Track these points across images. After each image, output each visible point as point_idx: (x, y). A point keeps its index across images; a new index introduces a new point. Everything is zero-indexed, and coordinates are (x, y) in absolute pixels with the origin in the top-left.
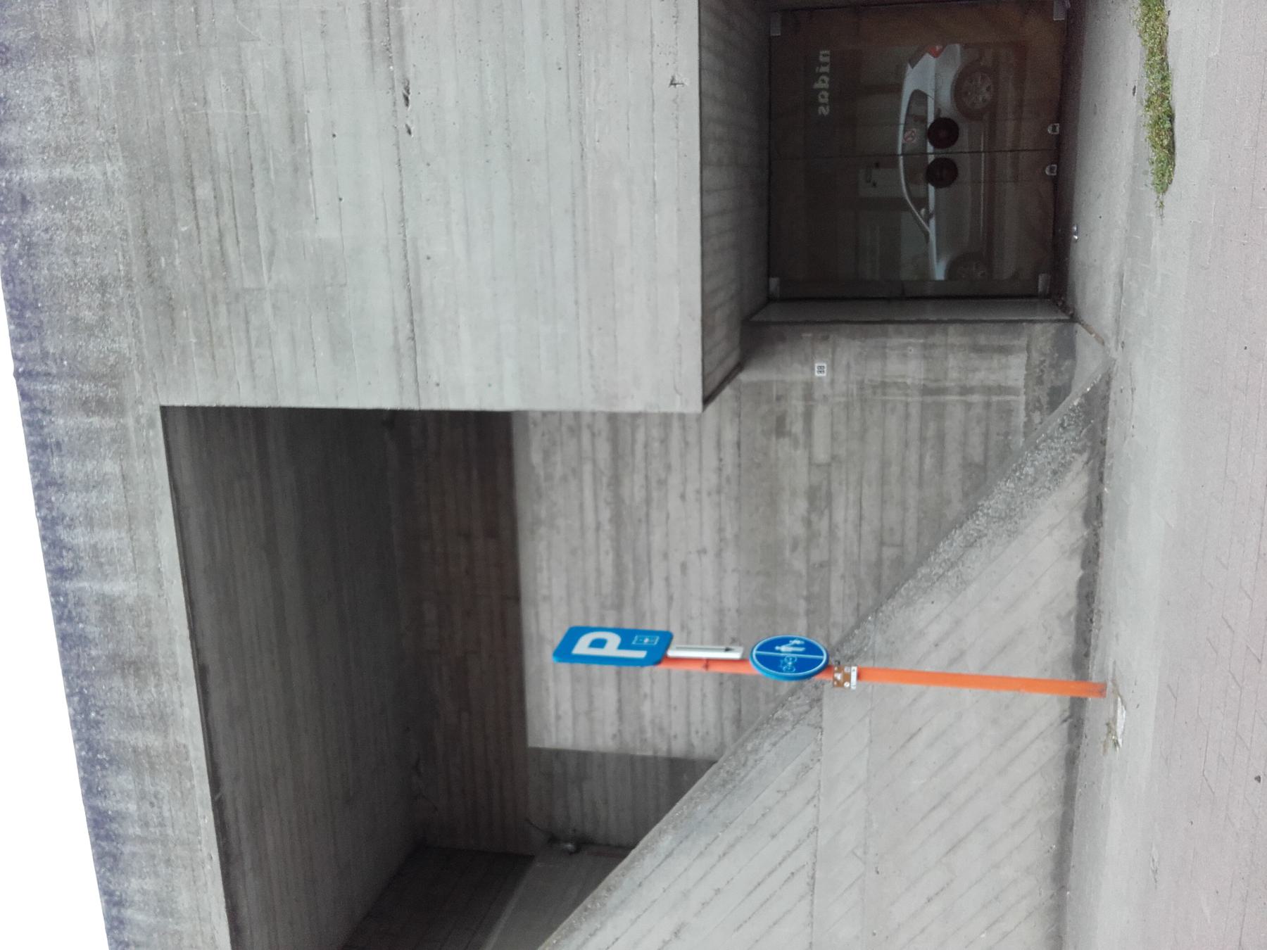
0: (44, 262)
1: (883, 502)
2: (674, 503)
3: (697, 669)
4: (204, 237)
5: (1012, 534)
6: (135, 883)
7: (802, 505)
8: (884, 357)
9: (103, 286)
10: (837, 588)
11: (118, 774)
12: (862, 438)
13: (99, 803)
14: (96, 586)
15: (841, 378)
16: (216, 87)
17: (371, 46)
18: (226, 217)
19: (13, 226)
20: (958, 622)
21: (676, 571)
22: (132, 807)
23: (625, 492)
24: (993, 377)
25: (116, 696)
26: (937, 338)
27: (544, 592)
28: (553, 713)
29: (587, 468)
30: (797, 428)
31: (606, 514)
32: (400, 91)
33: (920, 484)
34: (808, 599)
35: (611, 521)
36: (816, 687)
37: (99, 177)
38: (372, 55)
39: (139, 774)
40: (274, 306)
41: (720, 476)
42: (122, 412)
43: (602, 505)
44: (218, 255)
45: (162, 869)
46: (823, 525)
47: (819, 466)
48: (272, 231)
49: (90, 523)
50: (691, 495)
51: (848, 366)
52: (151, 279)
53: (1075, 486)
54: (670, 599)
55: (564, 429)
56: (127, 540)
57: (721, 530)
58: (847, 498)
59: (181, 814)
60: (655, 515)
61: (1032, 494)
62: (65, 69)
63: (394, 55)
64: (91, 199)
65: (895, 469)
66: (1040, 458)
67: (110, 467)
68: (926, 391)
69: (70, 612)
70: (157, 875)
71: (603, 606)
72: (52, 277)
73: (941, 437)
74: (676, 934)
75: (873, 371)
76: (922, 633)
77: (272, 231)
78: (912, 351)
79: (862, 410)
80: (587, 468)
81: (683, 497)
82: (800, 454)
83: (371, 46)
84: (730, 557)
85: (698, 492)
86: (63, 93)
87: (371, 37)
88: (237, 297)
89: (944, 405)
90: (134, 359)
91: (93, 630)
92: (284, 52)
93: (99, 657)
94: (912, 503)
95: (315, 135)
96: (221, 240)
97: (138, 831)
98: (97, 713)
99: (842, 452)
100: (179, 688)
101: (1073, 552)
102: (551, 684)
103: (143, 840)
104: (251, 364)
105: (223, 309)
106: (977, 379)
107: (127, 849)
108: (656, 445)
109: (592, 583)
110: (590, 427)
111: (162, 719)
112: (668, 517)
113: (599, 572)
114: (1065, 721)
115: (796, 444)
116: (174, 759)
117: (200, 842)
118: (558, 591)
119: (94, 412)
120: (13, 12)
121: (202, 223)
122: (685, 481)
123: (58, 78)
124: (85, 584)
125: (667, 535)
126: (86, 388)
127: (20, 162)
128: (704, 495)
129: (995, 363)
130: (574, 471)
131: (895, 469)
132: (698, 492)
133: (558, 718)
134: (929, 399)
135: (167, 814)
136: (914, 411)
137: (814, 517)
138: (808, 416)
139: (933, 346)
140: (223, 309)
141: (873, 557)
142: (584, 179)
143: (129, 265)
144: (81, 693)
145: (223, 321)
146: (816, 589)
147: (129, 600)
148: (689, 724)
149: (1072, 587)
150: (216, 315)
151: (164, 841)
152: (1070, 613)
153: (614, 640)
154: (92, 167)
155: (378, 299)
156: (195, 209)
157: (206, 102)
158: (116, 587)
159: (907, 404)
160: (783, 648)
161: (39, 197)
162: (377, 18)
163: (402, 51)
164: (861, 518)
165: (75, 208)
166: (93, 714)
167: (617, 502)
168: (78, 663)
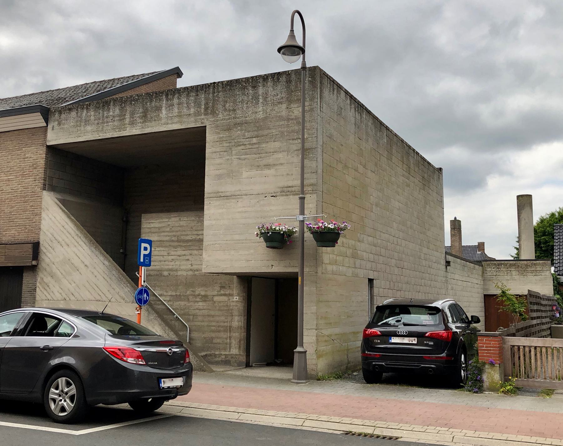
0: (240, 93)
4: (244, 140)
6: (92, 113)
7: (203, 293)
9: (234, 110)
10: (182, 303)
12: (219, 310)
14: (164, 105)
15: (234, 304)
16: (277, 144)
18: (248, 146)
21: (187, 258)
22: (111, 113)
26: (243, 330)
32: (274, 195)
33: (208, 326)
34: (180, 295)
39: (119, 116)
42: (205, 115)
45: (96, 122)
46: (198, 300)
48: (245, 159)
49: (179, 104)
52: (236, 124)
54: (180, 256)
56: (175, 115)
65: (211, 319)
67: (192, 110)
68: (230, 327)
70: (95, 120)
73: (219, 331)
74: (86, 265)
75: (236, 313)
76: (154, 328)
77: (245, 159)
84: (190, 273)
89: (227, 332)
91: (153, 104)
94: (203, 324)
95: (267, 172)
97: (105, 115)
99: (216, 304)
103: (103, 117)
104: (215, 152)
105: (228, 145)
106: (233, 341)
107: (101, 111)
109: (184, 233)
111: (132, 123)
118: (182, 223)
123: (282, 98)
124: (164, 102)
127: (264, 86)
129: (236, 346)
131: (211, 319)
133: (149, 223)
134: (228, 328)
135: (110, 124)
136: (226, 324)
138: (225, 295)
140: (228, 145)
141: (190, 313)
145: (225, 145)
146: (182, 297)
151: (103, 123)
153: (147, 252)
155: (229, 188)
158: (164, 111)
160: (145, 295)
163: (282, 195)
165: (252, 102)
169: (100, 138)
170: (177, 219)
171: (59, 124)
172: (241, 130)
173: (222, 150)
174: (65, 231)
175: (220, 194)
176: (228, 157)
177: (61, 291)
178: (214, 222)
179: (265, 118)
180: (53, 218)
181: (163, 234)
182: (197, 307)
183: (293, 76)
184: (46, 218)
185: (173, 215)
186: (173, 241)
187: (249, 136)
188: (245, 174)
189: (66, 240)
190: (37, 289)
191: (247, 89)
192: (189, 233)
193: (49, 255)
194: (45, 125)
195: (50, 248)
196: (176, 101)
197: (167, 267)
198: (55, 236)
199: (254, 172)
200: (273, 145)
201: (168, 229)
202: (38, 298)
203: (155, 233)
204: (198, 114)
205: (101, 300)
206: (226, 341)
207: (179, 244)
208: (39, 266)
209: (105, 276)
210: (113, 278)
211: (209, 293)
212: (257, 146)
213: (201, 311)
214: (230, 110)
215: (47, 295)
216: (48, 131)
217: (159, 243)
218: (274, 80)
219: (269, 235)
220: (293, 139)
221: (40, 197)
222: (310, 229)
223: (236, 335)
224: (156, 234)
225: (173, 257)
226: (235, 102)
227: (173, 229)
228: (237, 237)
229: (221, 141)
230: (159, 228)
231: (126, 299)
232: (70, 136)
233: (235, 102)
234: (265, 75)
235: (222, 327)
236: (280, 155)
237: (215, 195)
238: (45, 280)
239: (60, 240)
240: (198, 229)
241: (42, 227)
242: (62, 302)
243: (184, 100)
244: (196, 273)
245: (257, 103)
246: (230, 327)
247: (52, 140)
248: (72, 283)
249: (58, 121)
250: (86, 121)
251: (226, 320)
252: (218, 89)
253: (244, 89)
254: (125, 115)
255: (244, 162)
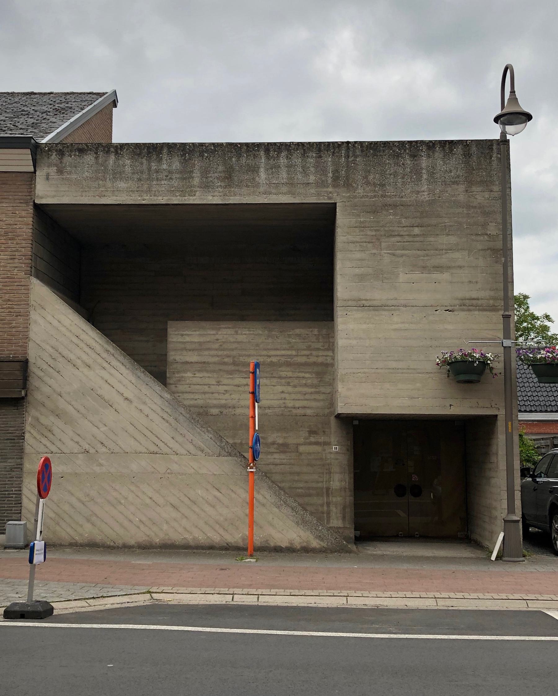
1: (283, 474)
2: (280, 388)
3: (251, 414)
4: (400, 229)
5: (297, 523)
6: (128, 162)
7: (280, 441)
8: (341, 473)
9: (383, 185)
11: (180, 162)
13: (165, 150)
14: (262, 165)
15: (332, 456)
16: (453, 239)
17: (465, 299)
18: (407, 238)
19: (405, 150)
20: (263, 505)
22: (165, 166)
23: (283, 369)
24: (334, 514)
25: (215, 167)
27: (239, 332)
28: (184, 333)
29: (294, 353)
30: (312, 439)
31: (274, 360)
32: (450, 308)
33: (290, 488)
35: (271, 361)
36: (235, 454)
37: (422, 189)
38: (462, 300)
40: (375, 254)
41: (292, 408)
42: (334, 186)
43: (278, 358)
44: (393, 234)
46: (272, 450)
47: (297, 447)
48: (402, 256)
50: (283, 395)
51: (337, 459)
52: (385, 206)
53: (315, 543)
54: (238, 386)
55: (310, 343)
57: (269, 408)
58: (284, 459)
59: (163, 189)
60: (275, 380)
61: (312, 529)
62: (461, 180)
63: (462, 307)
64: (414, 185)
65: (296, 478)
66: (325, 532)
67: (312, 178)
68: (328, 489)
69: (251, 151)
71: (234, 357)
72: (386, 164)
73: (310, 495)
74: (126, 399)
75: (335, 469)
77: (402, 256)
78: (343, 483)
79: (320, 465)
80: (294, 353)
81: (283, 392)
82: (302, 440)
83: (465, 299)
85: (285, 399)
86: (453, 178)
87: (468, 299)
88: (378, 239)
90: (355, 194)
91: (243, 160)
92: (464, 267)
93: (232, 161)
95: (436, 276)
96: (399, 235)
97: (154, 168)
98: (207, 157)
100: (220, 196)
101: (291, 544)
102: (198, 333)
103: (149, 169)
105: (374, 233)
106: (333, 509)
107: (144, 161)
108: (304, 382)
110: (311, 354)
111: (206, 186)
112: (274, 386)
113: (249, 356)
114: (227, 544)
115: (306, 438)
116: (189, 189)
117: (151, 196)
118: (240, 338)
119: (333, 174)
120: (482, 161)
121: (405, 229)
122: (289, 393)
123: (458, 177)
125: (266, 385)
126: (343, 172)
127: (429, 156)
128: (283, 401)
130: (292, 347)
131: (296, 478)
132: (285, 399)
133: (182, 335)
134: (325, 490)
135: (163, 182)
136: (320, 485)
137: (275, 446)
138: (317, 443)
139: (345, 491)
142: (419, 373)
143: (390, 197)
144: (216, 151)
145: (369, 233)
147: (257, 179)
148: (183, 393)
149: (279, 544)
150: (370, 230)
151: (149, 179)
152: (268, 544)
154: (426, 186)
155: (379, 295)
156: (410, 227)
157: (448, 235)
158: (263, 175)
159: (323, 482)
161: (416, 163)
162: (474, 302)
163: (463, 310)
164: (276, 465)
166: (206, 155)
167: (280, 365)
168: (228, 151)
169: (144, 202)
170: (229, 331)
171: (60, 171)
172: (395, 214)
173: (364, 240)
174: (82, 345)
175: (364, 302)
176: (374, 251)
177: (77, 439)
178: (354, 342)
179: (432, 203)
180: (55, 323)
181: (206, 353)
182: (272, 461)
183: (474, 149)
184: (41, 321)
185: (223, 324)
186: (225, 364)
187: (407, 224)
188: (402, 277)
189: (84, 357)
190: (27, 436)
191: (402, 158)
192: (252, 352)
193: (51, 382)
194: (32, 169)
195: (51, 370)
196: (283, 161)
197: (215, 402)
198: (60, 350)
199: (417, 276)
200: (444, 240)
201: (216, 346)
202: (28, 449)
203: (193, 350)
204: (321, 184)
205: (160, 452)
206: (320, 509)
207: (237, 368)
208: (30, 398)
209: (165, 416)
210: (181, 418)
211: (292, 440)
212: (421, 239)
213: (278, 467)
214: (375, 185)
215: (48, 444)
216: (38, 180)
217: (200, 365)
218: (444, 150)
219: (475, 365)
220: (477, 235)
221: (27, 288)
222: (525, 360)
223: (337, 499)
224: (196, 353)
225: (226, 388)
226: (383, 173)
227: (225, 346)
228: (394, 365)
229: (362, 227)
230: (200, 343)
231: (207, 450)
232: (84, 194)
233: (383, 173)
234: (431, 141)
235: (316, 488)
236: (456, 255)
237: (354, 303)
238: (43, 420)
239: (72, 357)
240: (269, 347)
241: (32, 335)
242: (80, 456)
243: (283, 161)
244: (267, 411)
245: (419, 179)
246: (328, 489)
247: (47, 196)
248: (101, 425)
249: (56, 165)
250: (114, 174)
251: (321, 480)
252: (354, 152)
253: (398, 156)
254: (192, 172)
255: (401, 260)
